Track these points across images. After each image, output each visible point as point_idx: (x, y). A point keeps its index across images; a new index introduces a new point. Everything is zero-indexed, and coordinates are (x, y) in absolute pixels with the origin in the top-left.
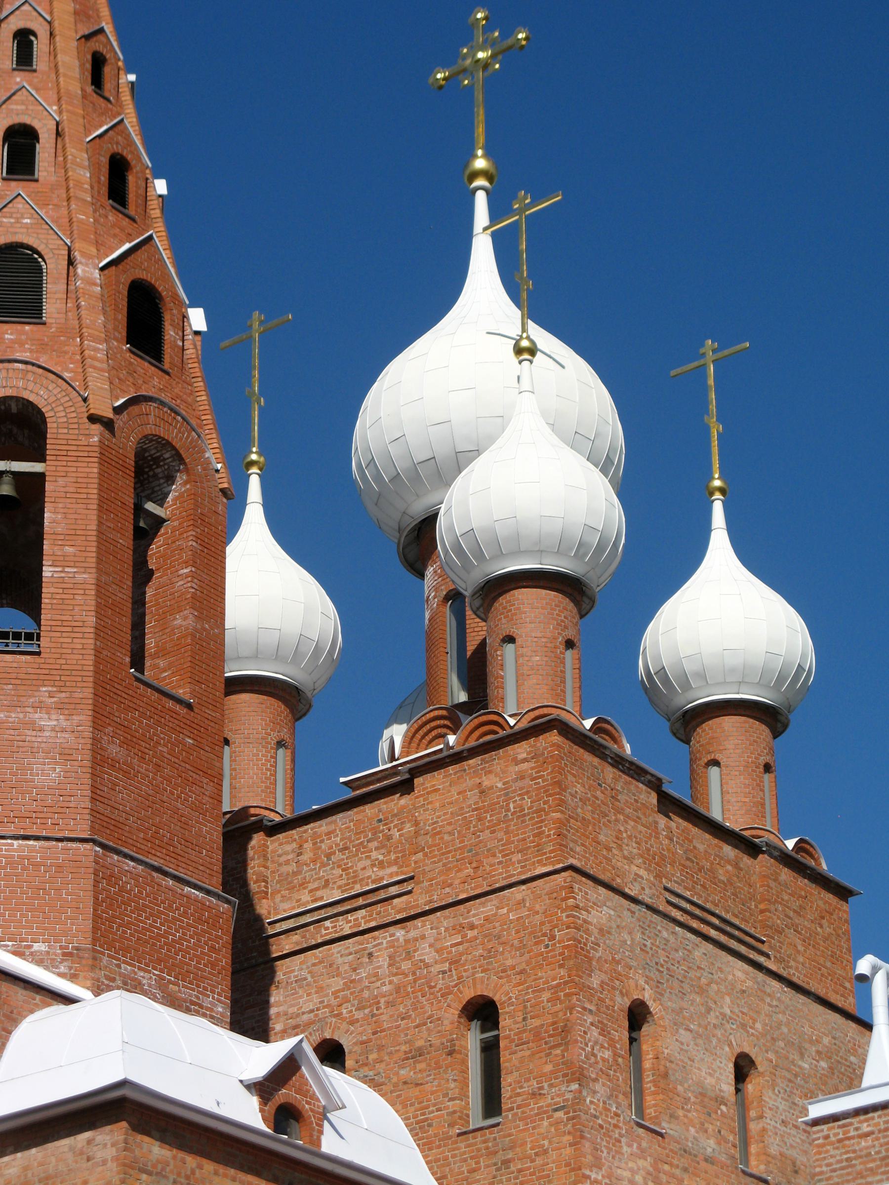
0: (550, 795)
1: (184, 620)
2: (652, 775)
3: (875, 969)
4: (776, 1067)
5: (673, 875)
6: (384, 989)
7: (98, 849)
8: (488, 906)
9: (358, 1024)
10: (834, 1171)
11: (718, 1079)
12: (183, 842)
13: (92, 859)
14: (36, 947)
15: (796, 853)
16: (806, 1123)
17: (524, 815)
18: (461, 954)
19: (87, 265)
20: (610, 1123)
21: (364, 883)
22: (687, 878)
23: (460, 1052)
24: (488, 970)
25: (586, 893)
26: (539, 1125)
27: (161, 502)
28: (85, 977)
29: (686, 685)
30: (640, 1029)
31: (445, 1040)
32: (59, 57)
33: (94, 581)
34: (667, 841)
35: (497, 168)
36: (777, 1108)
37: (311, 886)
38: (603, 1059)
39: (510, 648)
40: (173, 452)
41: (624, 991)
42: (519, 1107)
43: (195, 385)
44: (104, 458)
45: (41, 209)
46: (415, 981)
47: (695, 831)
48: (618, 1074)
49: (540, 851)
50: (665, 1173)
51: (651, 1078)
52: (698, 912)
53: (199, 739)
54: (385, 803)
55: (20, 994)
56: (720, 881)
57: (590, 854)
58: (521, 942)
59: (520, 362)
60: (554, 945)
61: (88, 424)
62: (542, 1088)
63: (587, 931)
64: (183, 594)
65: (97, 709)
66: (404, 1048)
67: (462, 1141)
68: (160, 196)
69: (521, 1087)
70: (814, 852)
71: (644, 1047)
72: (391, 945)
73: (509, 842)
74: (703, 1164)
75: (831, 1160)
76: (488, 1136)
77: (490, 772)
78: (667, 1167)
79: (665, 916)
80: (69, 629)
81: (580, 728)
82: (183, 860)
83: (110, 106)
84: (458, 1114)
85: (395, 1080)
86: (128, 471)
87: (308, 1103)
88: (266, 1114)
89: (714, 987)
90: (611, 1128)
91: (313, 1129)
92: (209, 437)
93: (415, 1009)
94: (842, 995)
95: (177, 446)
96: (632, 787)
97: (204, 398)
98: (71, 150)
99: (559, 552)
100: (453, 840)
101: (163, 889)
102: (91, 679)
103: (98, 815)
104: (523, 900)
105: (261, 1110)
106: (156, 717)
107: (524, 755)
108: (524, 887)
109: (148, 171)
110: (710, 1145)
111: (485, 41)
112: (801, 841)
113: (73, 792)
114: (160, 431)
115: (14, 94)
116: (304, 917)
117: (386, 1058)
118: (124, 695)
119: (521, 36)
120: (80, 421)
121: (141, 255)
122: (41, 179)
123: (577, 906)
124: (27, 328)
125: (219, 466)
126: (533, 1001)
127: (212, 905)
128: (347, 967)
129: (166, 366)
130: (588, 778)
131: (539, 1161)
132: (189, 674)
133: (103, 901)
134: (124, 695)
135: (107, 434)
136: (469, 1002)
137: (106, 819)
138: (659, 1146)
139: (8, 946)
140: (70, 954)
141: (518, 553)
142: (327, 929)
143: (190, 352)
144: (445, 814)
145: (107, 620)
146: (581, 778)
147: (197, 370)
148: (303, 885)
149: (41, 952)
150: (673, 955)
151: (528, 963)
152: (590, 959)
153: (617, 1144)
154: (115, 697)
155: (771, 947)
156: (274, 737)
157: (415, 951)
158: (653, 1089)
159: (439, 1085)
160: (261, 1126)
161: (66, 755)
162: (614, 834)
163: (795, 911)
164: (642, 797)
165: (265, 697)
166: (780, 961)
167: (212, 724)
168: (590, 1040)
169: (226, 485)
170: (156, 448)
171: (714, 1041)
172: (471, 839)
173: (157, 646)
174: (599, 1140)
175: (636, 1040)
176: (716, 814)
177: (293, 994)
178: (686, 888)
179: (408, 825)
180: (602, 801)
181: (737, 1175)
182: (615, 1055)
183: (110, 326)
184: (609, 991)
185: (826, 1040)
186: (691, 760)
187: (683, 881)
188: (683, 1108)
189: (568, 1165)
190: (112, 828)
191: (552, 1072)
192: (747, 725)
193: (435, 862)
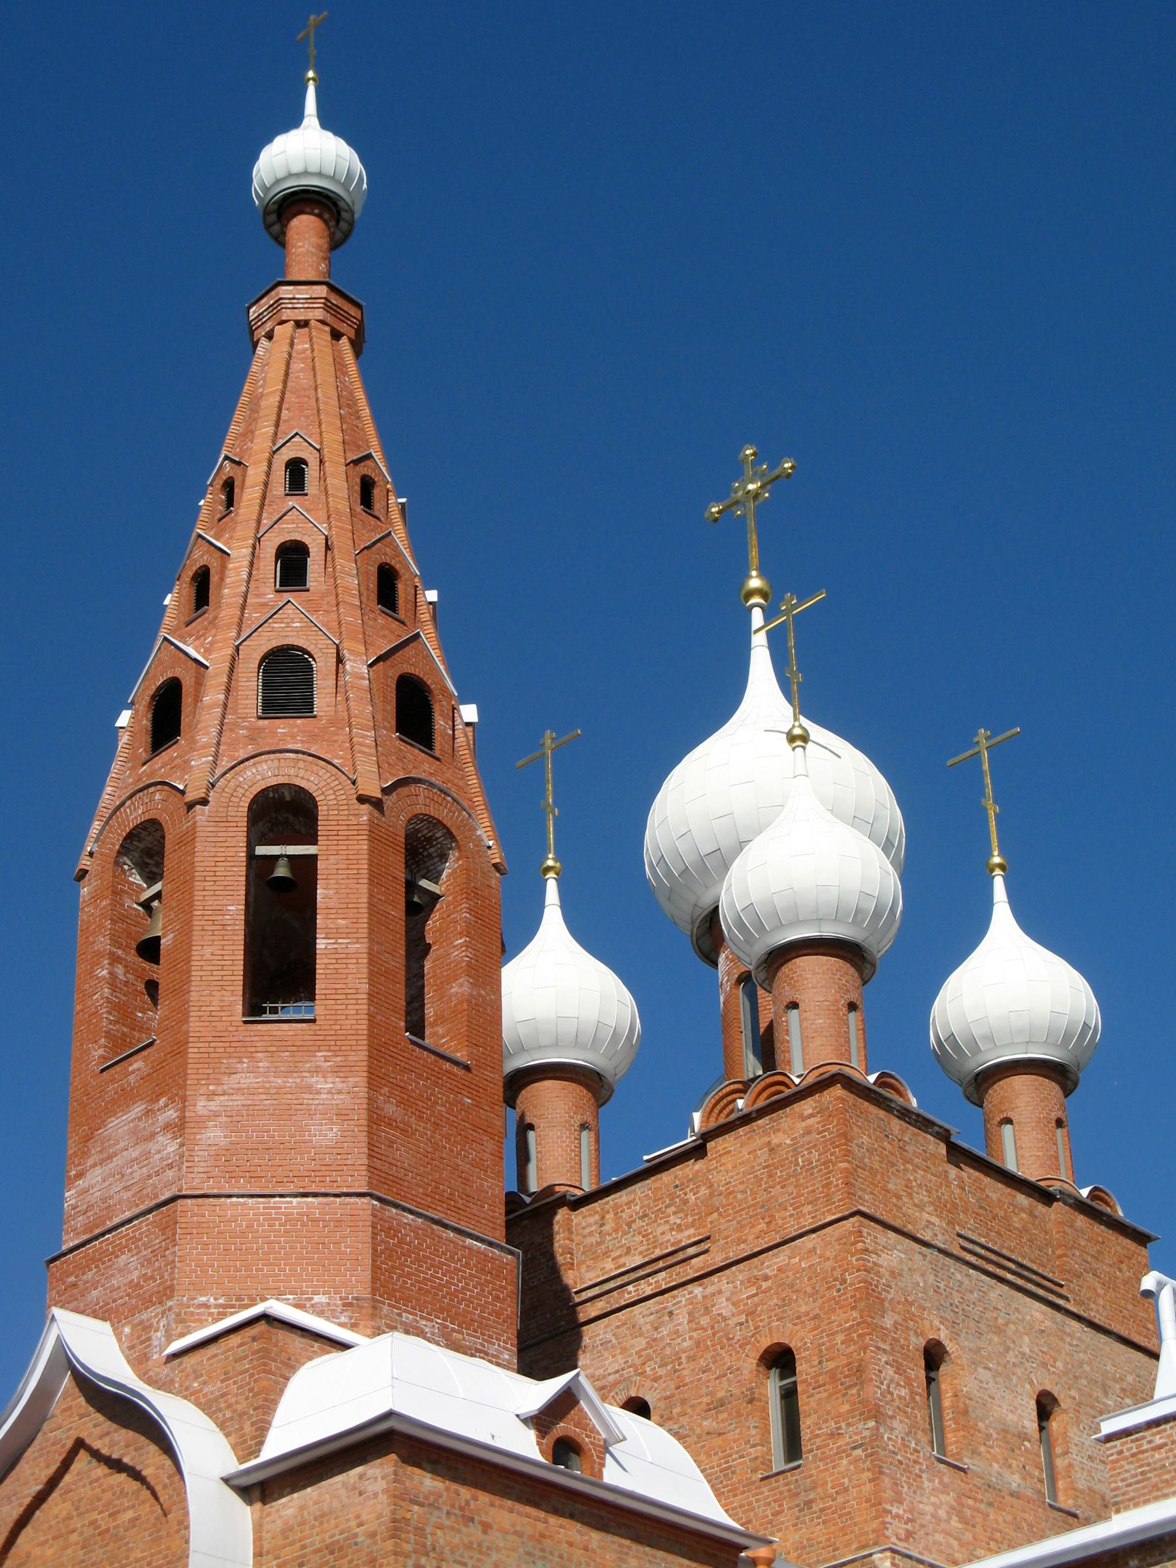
0: (837, 1147)
1: (460, 988)
2: (940, 1127)
3: (1161, 1285)
4: (1079, 1404)
5: (966, 1223)
6: (685, 1344)
7: (375, 1202)
8: (780, 1257)
9: (662, 1381)
10: (1130, 1485)
11: (1020, 1416)
12: (464, 1197)
13: (369, 1212)
14: (317, 1299)
15: (1092, 1200)
16: (1098, 1440)
17: (813, 1168)
18: (757, 1305)
19: (355, 661)
20: (909, 1460)
21: (664, 1247)
22: (981, 1225)
23: (760, 1400)
25: (876, 1237)
26: (838, 1464)
27: (435, 879)
28: (365, 1326)
29: (976, 1050)
30: (938, 1369)
31: (744, 1389)
32: (328, 482)
33: (366, 951)
34: (957, 1191)
35: (771, 587)
36: (1083, 1444)
37: (614, 1254)
38: (900, 1397)
39: (794, 1013)
40: (445, 831)
43: (467, 770)
44: (374, 835)
45: (312, 615)
46: (714, 1334)
47: (987, 1180)
48: (916, 1412)
49: (829, 1202)
50: (969, 1507)
52: (993, 1257)
53: (477, 1099)
54: (681, 1169)
55: (297, 1342)
56: (1015, 1228)
57: (880, 1202)
58: (814, 1288)
59: (794, 749)
60: (846, 1288)
61: (357, 805)
62: (840, 1428)
63: (877, 1273)
64: (459, 963)
65: (372, 1071)
66: (705, 1400)
67: (765, 1486)
68: (431, 603)
69: (820, 1429)
70: (1109, 1200)
71: (943, 1386)
72: (690, 1302)
73: (799, 1195)
74: (1008, 1499)
75: (1127, 1475)
76: (790, 1478)
77: (778, 1130)
78: (970, 1502)
79: (958, 1259)
80: (344, 997)
81: (865, 1084)
82: (464, 1214)
83: (379, 523)
84: (761, 1459)
85: (698, 1431)
86: (398, 848)
87: (587, 1436)
88: (544, 1447)
89: (1012, 1327)
90: (911, 1463)
91: (594, 1462)
92: (480, 817)
94: (1145, 1337)
95: (448, 825)
96: (920, 1139)
97: (474, 781)
98: (339, 561)
99: (837, 919)
100: (746, 1197)
101: (444, 1241)
102: (366, 1042)
103: (375, 1171)
104: (814, 1248)
105: (539, 1443)
106: (433, 1078)
107: (810, 1111)
108: (814, 1236)
109: (416, 580)
110: (1015, 1481)
111: (755, 474)
112: (1095, 1189)
114: (430, 811)
115: (285, 515)
116: (608, 1284)
117: (689, 1410)
118: (400, 1057)
120: (350, 802)
121: (409, 651)
123: (867, 1250)
124: (299, 721)
125: (491, 843)
126: (828, 1344)
127: (495, 1257)
128: (649, 1327)
129: (437, 753)
130: (875, 1130)
131: (840, 1499)
132: (466, 1038)
133: (381, 1253)
134: (400, 1057)
135: (376, 813)
136: (766, 1351)
137: (384, 1175)
138: (962, 1481)
139: (289, 1299)
140: (350, 1305)
141: (797, 922)
142: (630, 1293)
143: (461, 740)
144: (738, 1174)
145: (380, 987)
146: (866, 1130)
147: (468, 756)
148: (606, 1254)
149: (321, 1304)
150: (968, 1296)
151: (821, 1308)
153: (918, 1479)
154: (391, 1059)
155: (1070, 1291)
156: (577, 1120)
157: (713, 1306)
158: (953, 1426)
159: (741, 1433)
160: (540, 1458)
161: (342, 1115)
162: (904, 1183)
163: (1092, 1256)
164: (931, 1147)
165: (567, 1083)
166: (1079, 1303)
167: (492, 1085)
168: (885, 1379)
169: (498, 860)
170: (428, 828)
171: (1014, 1379)
172: (762, 1196)
173: (435, 1014)
175: (934, 1380)
176: (1011, 1165)
177: (599, 1357)
178: (980, 1235)
179: (703, 1188)
180: (890, 1152)
181: (1045, 1510)
182: (912, 1393)
183: (379, 717)
184: (903, 1331)
185: (1130, 1379)
186: (985, 1121)
187: (976, 1227)
188: (985, 1444)
189: (868, 1500)
190: (390, 1183)
192: (1037, 1083)
193: (729, 1221)
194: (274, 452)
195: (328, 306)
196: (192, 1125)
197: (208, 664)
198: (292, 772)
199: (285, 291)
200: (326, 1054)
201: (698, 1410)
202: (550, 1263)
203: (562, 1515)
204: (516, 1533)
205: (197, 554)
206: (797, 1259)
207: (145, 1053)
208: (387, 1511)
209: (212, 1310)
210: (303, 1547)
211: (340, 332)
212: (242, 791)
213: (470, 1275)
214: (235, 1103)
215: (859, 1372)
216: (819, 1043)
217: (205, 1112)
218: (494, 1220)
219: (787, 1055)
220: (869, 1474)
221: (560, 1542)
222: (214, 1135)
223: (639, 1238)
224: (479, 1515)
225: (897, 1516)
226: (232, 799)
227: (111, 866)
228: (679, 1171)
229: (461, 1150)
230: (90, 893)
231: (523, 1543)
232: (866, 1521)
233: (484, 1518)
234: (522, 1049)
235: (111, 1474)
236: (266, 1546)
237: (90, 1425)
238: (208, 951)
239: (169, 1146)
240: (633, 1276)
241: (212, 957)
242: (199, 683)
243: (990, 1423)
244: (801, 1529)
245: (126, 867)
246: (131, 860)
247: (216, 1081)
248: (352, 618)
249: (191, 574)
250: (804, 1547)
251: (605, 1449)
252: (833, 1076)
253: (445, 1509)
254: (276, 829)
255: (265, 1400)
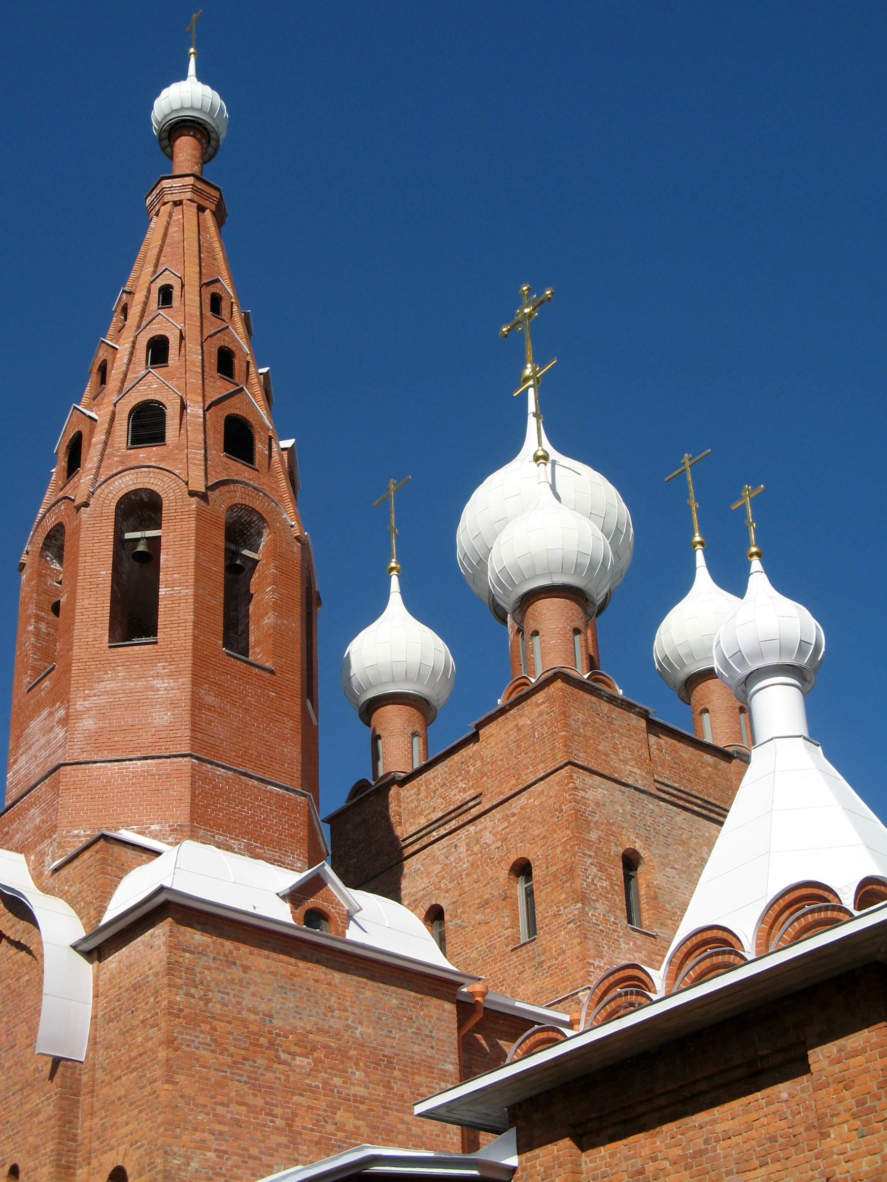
2: (640, 708)
5: (663, 773)
8: (522, 800)
13: (189, 767)
14: (153, 827)
18: (508, 834)
19: (194, 407)
20: (609, 929)
24: (524, 840)
27: (256, 551)
29: (682, 664)
30: (636, 870)
37: (425, 813)
38: (602, 887)
41: (618, 843)
42: (546, 926)
45: (168, 381)
46: (482, 857)
47: (679, 745)
51: (645, 900)
52: (684, 796)
55: (130, 853)
58: (543, 818)
59: (538, 465)
62: (559, 910)
63: (585, 804)
66: (477, 901)
69: (547, 913)
71: (640, 881)
72: (467, 837)
73: (536, 757)
77: (523, 716)
79: (651, 795)
80: (177, 625)
85: (473, 923)
88: (297, 915)
90: (611, 932)
93: (482, 876)
96: (625, 716)
107: (542, 700)
108: (542, 782)
113: (179, 727)
117: (467, 910)
119: (548, 293)
121: (235, 400)
122: (170, 365)
123: (576, 788)
124: (154, 449)
125: (293, 523)
128: (442, 857)
129: (257, 467)
131: (560, 958)
135: (202, 503)
137: (203, 743)
139: (133, 829)
140: (176, 830)
141: (536, 576)
143: (275, 457)
148: (421, 813)
150: (658, 819)
151: (547, 831)
152: (589, 823)
154: (211, 666)
156: (409, 731)
157: (481, 838)
158: (647, 907)
161: (173, 704)
167: (292, 684)
168: (590, 875)
169: (298, 534)
173: (255, 640)
174: (600, 940)
175: (633, 877)
176: (708, 739)
182: (612, 884)
184: (605, 843)
187: (672, 777)
188: (671, 919)
189: (578, 957)
191: (565, 899)
194: (152, 282)
195: (195, 190)
196: (73, 718)
197: (96, 417)
198: (146, 480)
199: (166, 183)
200: (164, 664)
201: (473, 908)
202: (387, 824)
203: (311, 961)
204: (270, 973)
205: (101, 353)
206: (532, 800)
207: (49, 675)
208: (165, 959)
209: (82, 839)
210: (120, 988)
211: (204, 207)
212: (112, 496)
213: (271, 810)
214: (102, 701)
215: (571, 871)
216: (552, 656)
217: (82, 709)
218: (292, 774)
219: (532, 667)
220: (578, 940)
221: (307, 980)
222: (88, 723)
223: (440, 800)
224: (239, 960)
225: (599, 967)
226: (105, 501)
227: (37, 558)
228: (465, 752)
229: (267, 727)
230: (26, 578)
231: (277, 980)
232: (577, 971)
233: (244, 962)
234: (371, 686)
235: (17, 953)
236: (101, 990)
237: (6, 921)
238: (87, 602)
239: (60, 733)
240: (436, 825)
241: (90, 606)
242: (92, 433)
243: (676, 905)
244: (536, 981)
245: (48, 559)
246: (52, 554)
247: (90, 688)
248: (195, 380)
249: (97, 367)
250: (538, 993)
251: (349, 917)
252: (555, 674)
253: (212, 956)
254: (144, 523)
255: (103, 892)
